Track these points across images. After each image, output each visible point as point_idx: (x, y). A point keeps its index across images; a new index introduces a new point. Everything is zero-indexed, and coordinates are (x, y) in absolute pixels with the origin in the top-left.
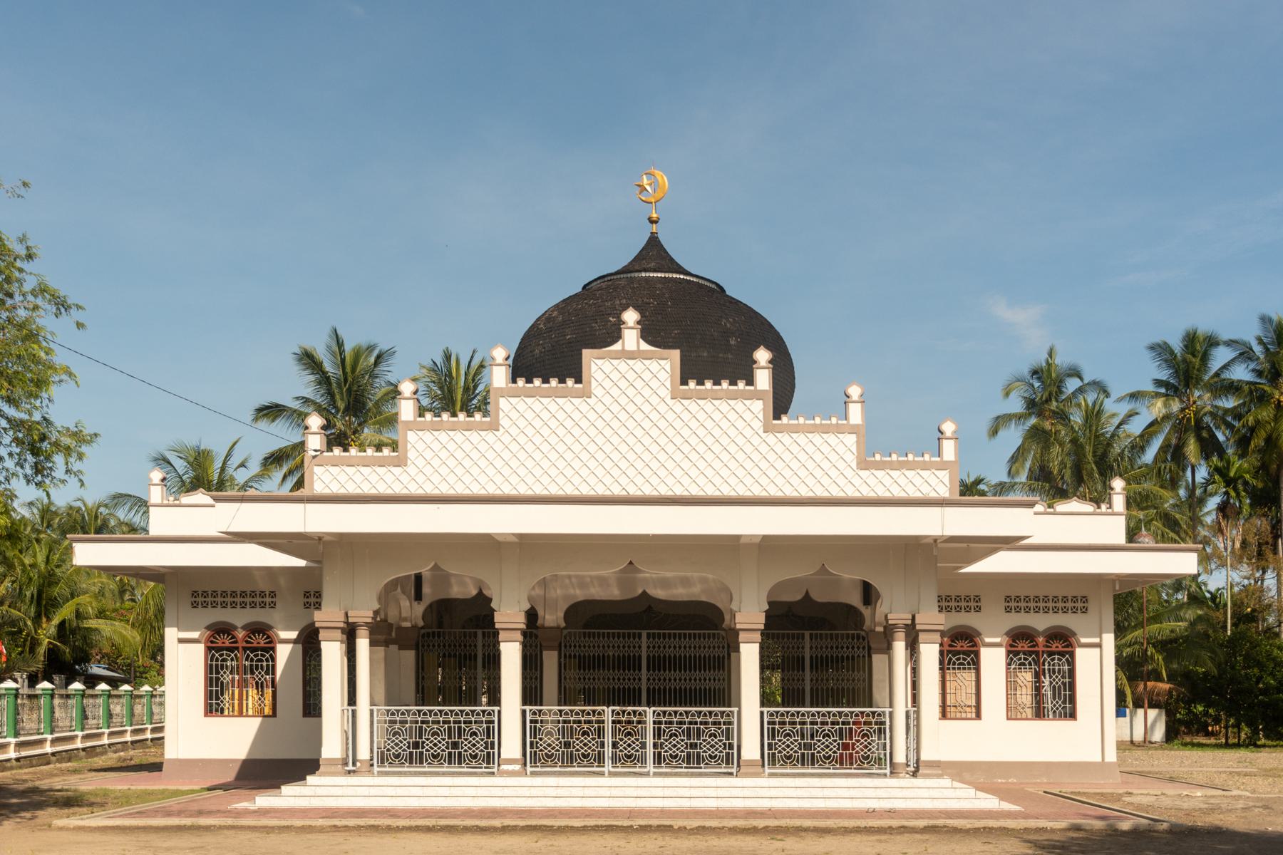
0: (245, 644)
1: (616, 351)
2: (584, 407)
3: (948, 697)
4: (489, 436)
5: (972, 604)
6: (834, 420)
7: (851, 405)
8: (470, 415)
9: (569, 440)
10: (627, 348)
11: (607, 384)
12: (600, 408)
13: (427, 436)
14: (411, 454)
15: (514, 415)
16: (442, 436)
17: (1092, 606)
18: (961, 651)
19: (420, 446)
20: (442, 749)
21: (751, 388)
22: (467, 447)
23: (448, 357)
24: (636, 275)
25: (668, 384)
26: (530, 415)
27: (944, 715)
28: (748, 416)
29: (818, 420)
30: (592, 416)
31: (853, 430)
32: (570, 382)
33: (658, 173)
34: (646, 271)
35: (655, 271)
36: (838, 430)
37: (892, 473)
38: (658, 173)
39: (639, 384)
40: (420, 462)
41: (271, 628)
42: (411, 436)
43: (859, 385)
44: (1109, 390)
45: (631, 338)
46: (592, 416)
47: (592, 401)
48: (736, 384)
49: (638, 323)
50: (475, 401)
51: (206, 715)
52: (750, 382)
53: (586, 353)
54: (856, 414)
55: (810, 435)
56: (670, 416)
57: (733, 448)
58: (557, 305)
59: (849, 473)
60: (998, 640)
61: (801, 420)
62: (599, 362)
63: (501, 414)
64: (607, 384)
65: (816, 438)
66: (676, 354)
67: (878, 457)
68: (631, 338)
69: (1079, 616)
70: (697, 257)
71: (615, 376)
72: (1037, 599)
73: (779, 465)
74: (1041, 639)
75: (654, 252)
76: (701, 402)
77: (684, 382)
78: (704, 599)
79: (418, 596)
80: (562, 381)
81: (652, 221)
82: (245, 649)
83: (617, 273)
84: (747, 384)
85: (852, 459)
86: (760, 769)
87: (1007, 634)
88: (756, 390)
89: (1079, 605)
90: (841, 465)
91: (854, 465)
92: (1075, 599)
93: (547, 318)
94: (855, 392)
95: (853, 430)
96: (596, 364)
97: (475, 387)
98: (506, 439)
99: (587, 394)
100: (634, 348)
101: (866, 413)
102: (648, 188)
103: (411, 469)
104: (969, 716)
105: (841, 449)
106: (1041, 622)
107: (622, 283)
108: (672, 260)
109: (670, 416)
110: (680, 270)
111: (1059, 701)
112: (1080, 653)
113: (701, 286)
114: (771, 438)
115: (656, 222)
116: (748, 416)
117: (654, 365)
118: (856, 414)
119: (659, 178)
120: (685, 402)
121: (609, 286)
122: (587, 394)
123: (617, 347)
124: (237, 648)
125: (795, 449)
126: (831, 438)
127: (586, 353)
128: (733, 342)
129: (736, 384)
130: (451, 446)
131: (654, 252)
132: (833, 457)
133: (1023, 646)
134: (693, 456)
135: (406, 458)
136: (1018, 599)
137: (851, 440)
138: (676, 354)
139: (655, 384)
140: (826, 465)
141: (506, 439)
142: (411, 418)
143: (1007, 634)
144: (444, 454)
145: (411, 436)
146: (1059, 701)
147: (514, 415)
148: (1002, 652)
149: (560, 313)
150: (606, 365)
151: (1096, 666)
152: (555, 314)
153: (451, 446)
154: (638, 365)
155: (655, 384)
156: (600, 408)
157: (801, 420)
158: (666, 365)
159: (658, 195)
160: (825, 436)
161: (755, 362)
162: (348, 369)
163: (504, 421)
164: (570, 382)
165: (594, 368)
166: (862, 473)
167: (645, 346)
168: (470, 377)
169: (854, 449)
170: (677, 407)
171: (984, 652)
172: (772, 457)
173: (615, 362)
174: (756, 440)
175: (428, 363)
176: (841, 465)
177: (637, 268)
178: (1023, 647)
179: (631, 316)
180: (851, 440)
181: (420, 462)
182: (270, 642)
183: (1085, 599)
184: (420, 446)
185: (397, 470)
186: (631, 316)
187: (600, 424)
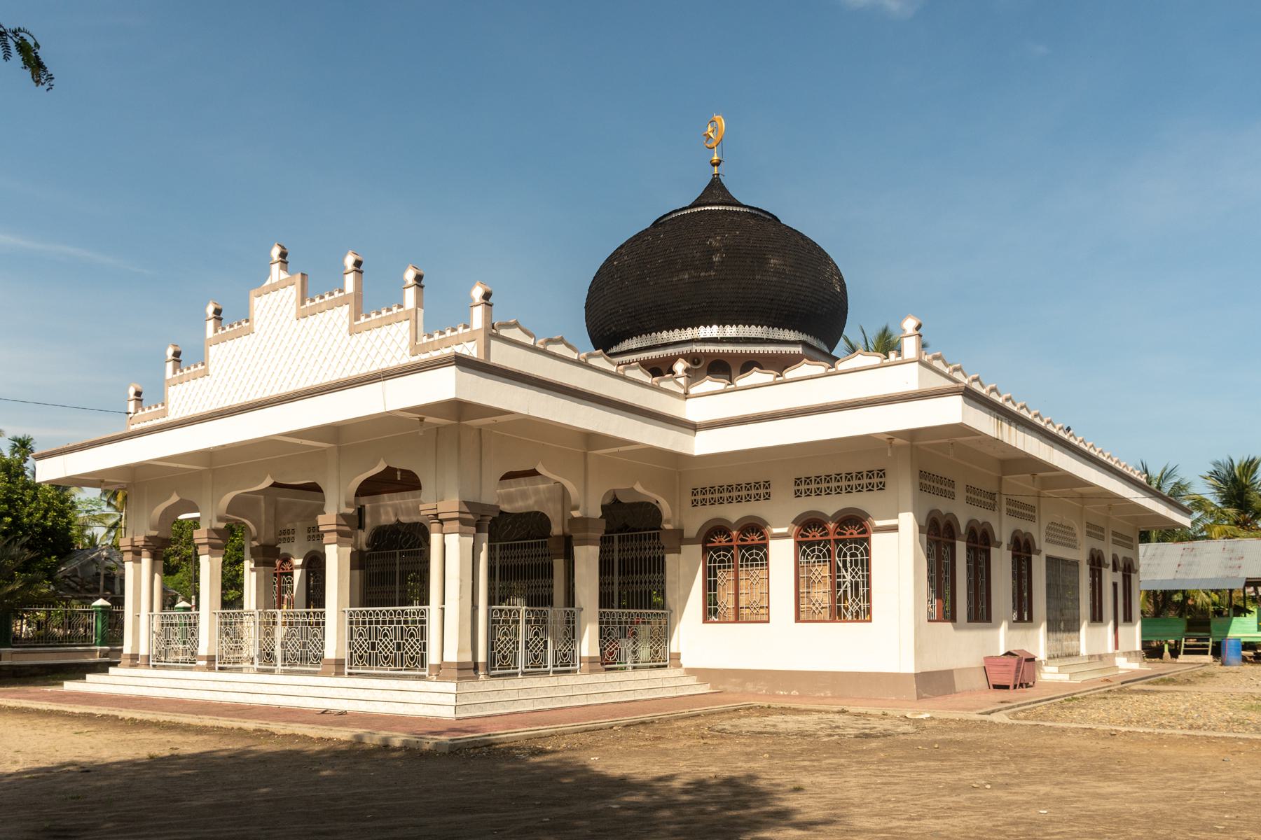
0: (740, 543)
3: (741, 597)
5: (762, 491)
17: (888, 480)
18: (748, 545)
20: (392, 652)
27: (798, 619)
41: (766, 524)
44: (810, 258)
51: (705, 620)
60: (785, 530)
69: (762, 502)
72: (828, 478)
74: (831, 526)
78: (536, 509)
79: (361, 526)
82: (837, 542)
86: (472, 673)
87: (795, 522)
89: (876, 480)
92: (870, 474)
104: (822, 617)
106: (830, 506)
111: (850, 602)
112: (876, 540)
115: (718, 164)
124: (732, 547)
133: (815, 534)
136: (808, 480)
143: (795, 522)
146: (850, 602)
148: (790, 543)
151: (897, 554)
171: (773, 544)
178: (810, 533)
182: (764, 539)
183: (882, 473)
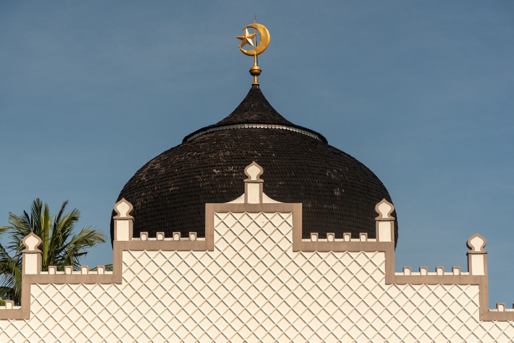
1: (240, 205)
2: (206, 261)
4: (112, 290)
6: (456, 272)
7: (474, 258)
8: (61, 268)
9: (190, 293)
10: (250, 201)
11: (230, 237)
12: (222, 261)
13: (50, 290)
14: (34, 308)
15: (136, 268)
16: (66, 290)
19: (43, 300)
21: (374, 240)
22: (89, 300)
23: (37, 208)
24: (239, 126)
25: (290, 237)
26: (152, 268)
28: (370, 268)
29: (440, 272)
30: (214, 269)
31: (476, 281)
32: (193, 236)
33: (261, 28)
34: (248, 123)
35: (258, 123)
36: (460, 281)
37: (499, 324)
38: (261, 28)
39: (261, 237)
40: (43, 316)
42: (34, 290)
43: (481, 236)
45: (254, 193)
46: (214, 269)
47: (214, 254)
48: (325, 237)
49: (261, 177)
50: (62, 254)
52: (372, 234)
53: (209, 207)
54: (478, 265)
55: (432, 287)
56: (292, 269)
57: (354, 300)
58: (159, 157)
59: (472, 324)
61: (424, 272)
62: (222, 216)
63: (124, 268)
64: (230, 237)
65: (439, 290)
66: (298, 207)
67: (501, 308)
68: (254, 193)
70: (300, 107)
71: (238, 229)
73: (402, 316)
75: (255, 103)
76: (323, 255)
77: (306, 235)
80: (185, 234)
81: (253, 73)
83: (219, 125)
84: (369, 237)
85: (474, 310)
88: (378, 242)
90: (464, 316)
91: (477, 316)
93: (148, 170)
94: (477, 243)
95: (476, 281)
96: (221, 220)
97: (65, 238)
98: (129, 292)
99: (209, 247)
100: (257, 202)
101: (487, 264)
102: (250, 40)
103: (33, 323)
105: (463, 300)
107: (226, 135)
108: (274, 112)
109: (292, 269)
110: (282, 121)
113: (305, 137)
114: (393, 290)
115: (258, 74)
116: (370, 268)
117: (277, 219)
118: (478, 265)
119: (262, 31)
120: (308, 255)
121: (212, 139)
122: (209, 247)
123: (240, 200)
125: (417, 300)
126: (454, 290)
127: (209, 207)
128: (337, 193)
129: (325, 237)
130: (74, 300)
131: (255, 103)
132: (456, 308)
134: (315, 309)
135: (29, 311)
137: (473, 291)
138: (298, 207)
139: (277, 237)
140: (448, 316)
141: (129, 292)
142: (35, 272)
144: (66, 308)
145: (34, 290)
147: (136, 268)
149: (162, 166)
150: (229, 220)
152: (157, 166)
153: (74, 300)
154: (260, 219)
155: (277, 237)
156: (222, 261)
157: (424, 272)
158: (286, 221)
159: (261, 47)
160: (447, 287)
161: (377, 215)
162: (59, 229)
163: (127, 275)
164: (193, 236)
165: (216, 221)
166: (484, 324)
167: (267, 200)
168: (59, 229)
169: (477, 300)
170: (300, 260)
172: (425, 308)
173: (238, 216)
174: (378, 292)
175: (20, 214)
176: (464, 316)
177: (239, 119)
179: (254, 171)
180: (473, 291)
181: (43, 316)
184: (43, 300)
185: (19, 324)
186: (254, 171)
187: (222, 277)
